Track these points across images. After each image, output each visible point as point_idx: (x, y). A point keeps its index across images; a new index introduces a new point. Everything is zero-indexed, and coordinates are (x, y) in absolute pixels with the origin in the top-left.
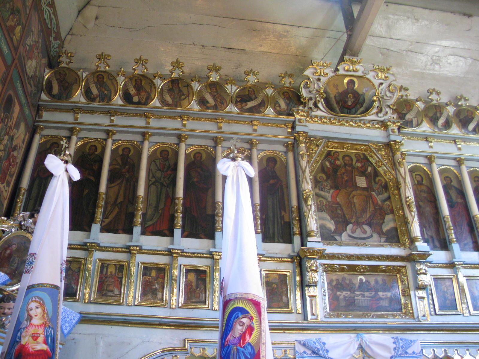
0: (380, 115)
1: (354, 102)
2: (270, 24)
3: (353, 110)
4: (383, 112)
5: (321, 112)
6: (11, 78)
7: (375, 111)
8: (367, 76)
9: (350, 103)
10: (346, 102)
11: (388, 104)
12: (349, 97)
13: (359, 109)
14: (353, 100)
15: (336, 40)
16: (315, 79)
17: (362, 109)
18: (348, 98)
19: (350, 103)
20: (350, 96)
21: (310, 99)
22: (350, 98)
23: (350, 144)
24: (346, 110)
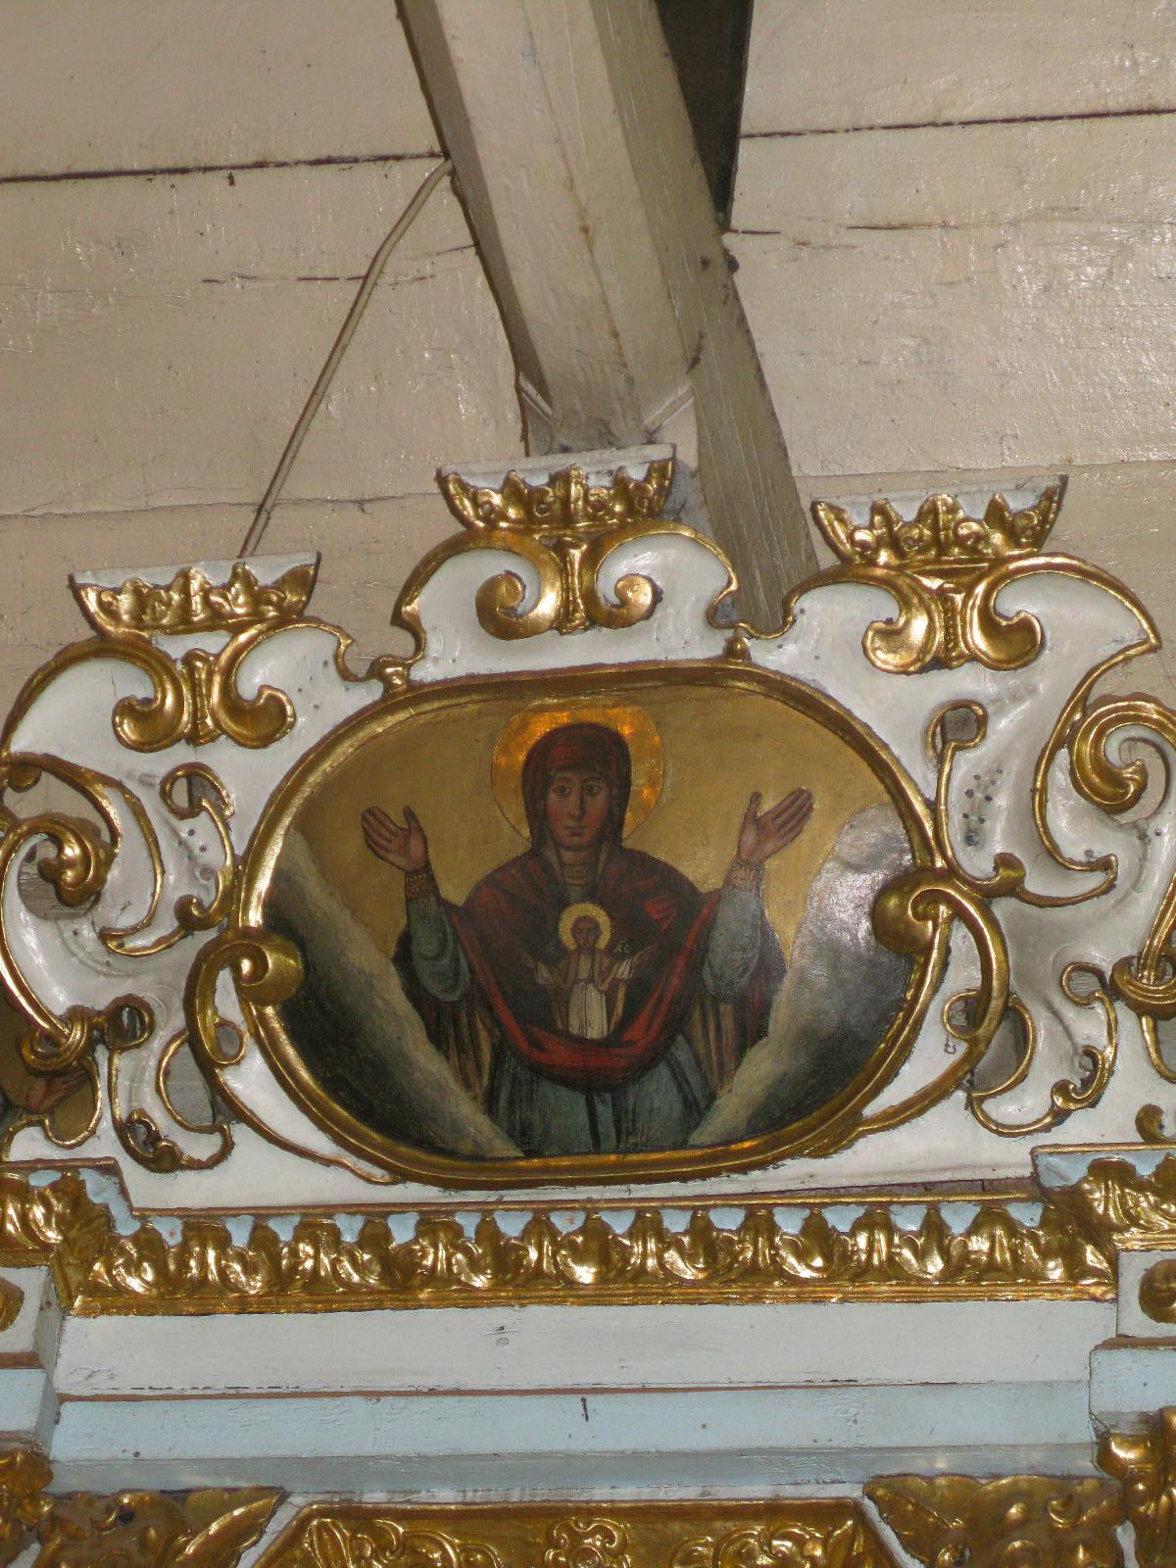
0: (1024, 1104)
1: (638, 992)
2: (987, 114)
3: (658, 1094)
4: (1047, 1067)
5: (281, 1161)
6: (1007, 992)
7: (931, 1055)
8: (776, 656)
9: (591, 1016)
10: (543, 1010)
11: (1103, 957)
12: (568, 939)
13: (725, 1074)
14: (624, 970)
15: (361, 281)
16: (145, 781)
17: (759, 1071)
18: (558, 956)
19: (591, 1016)
20: (585, 929)
21: (122, 1024)
22: (587, 947)
23: (616, 1512)
24: (567, 1108)
